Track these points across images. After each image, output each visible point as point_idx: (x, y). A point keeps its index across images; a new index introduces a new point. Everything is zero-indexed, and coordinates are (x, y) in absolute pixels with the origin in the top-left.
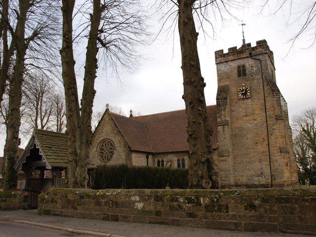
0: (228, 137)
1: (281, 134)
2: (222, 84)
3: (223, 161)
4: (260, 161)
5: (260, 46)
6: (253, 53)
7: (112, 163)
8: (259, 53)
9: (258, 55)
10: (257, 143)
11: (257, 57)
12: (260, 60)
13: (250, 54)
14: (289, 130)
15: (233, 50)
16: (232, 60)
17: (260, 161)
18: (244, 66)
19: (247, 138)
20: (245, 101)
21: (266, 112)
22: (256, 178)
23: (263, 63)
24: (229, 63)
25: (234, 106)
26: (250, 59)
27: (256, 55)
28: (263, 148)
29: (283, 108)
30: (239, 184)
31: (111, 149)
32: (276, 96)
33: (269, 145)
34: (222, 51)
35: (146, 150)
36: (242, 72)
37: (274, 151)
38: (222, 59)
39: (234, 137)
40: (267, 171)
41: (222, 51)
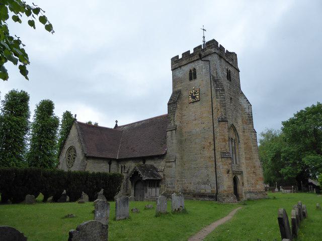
0: (175, 141)
1: (222, 137)
2: (176, 89)
3: (169, 167)
4: (207, 167)
5: (208, 47)
6: (203, 54)
7: (73, 169)
8: (208, 54)
9: (208, 55)
10: (204, 148)
11: (206, 59)
12: (209, 61)
13: (200, 55)
14: (253, 134)
15: (187, 55)
16: (185, 65)
17: (207, 167)
18: (195, 69)
19: (195, 143)
20: (196, 104)
21: (213, 115)
22: (203, 186)
23: (212, 63)
24: (182, 67)
25: (185, 110)
26: (200, 61)
27: (205, 56)
28: (209, 153)
29: (247, 110)
30: (188, 192)
31: (74, 155)
32: (220, 96)
33: (215, 150)
34: (177, 57)
35: (110, 156)
36: (193, 75)
37: (218, 156)
38: (177, 65)
39: (180, 142)
40: (213, 178)
41: (177, 57)
